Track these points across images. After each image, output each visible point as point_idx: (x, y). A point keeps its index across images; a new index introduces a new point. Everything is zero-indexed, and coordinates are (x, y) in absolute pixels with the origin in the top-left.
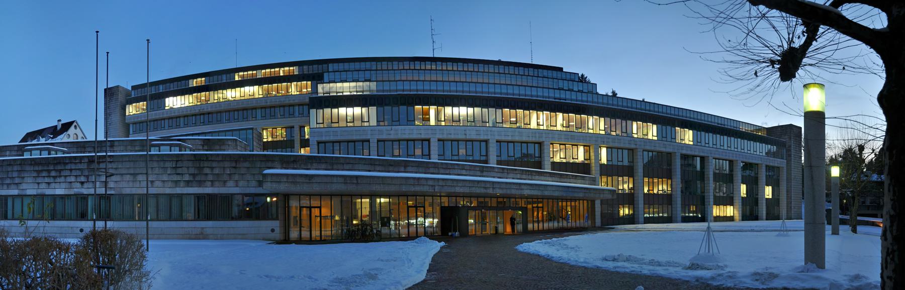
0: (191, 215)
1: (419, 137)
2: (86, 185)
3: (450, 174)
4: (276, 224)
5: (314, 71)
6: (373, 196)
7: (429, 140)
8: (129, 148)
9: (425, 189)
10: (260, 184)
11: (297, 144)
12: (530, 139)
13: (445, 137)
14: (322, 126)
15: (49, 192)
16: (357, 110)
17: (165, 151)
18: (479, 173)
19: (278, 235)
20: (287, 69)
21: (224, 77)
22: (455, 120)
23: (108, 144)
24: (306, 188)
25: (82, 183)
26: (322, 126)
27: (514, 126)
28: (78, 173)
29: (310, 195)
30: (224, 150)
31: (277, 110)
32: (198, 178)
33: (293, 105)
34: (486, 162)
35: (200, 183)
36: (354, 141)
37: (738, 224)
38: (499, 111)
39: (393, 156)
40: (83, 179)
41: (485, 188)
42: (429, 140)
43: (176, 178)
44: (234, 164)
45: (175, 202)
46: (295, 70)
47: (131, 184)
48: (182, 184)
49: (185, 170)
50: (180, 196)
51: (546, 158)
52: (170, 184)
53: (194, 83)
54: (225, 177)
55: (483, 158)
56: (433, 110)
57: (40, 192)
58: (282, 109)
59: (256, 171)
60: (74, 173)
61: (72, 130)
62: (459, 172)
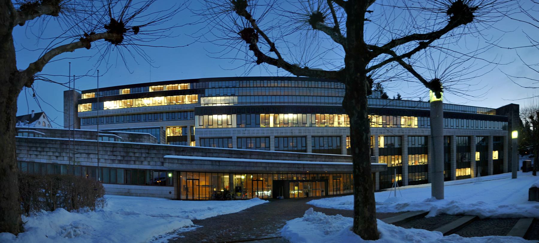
0: (123, 181)
2: (59, 158)
3: (278, 160)
4: (172, 189)
5: (199, 87)
6: (231, 174)
7: (269, 137)
8: (83, 136)
9: (261, 169)
10: (163, 163)
11: (189, 138)
13: (279, 135)
14: (202, 127)
15: (37, 160)
16: (224, 117)
17: (106, 140)
18: (297, 158)
19: (173, 195)
20: (183, 84)
21: (142, 88)
22: (285, 123)
23: (70, 132)
24: (189, 167)
25: (57, 157)
26: (202, 127)
27: (323, 126)
28: (54, 150)
30: (142, 142)
32: (126, 159)
33: (187, 112)
35: (128, 162)
36: (223, 138)
37: (473, 179)
38: (314, 116)
39: (247, 148)
40: (57, 154)
41: (298, 168)
42: (269, 137)
43: (113, 158)
44: (147, 151)
45: (112, 173)
46: (188, 86)
47: (86, 160)
48: (117, 162)
49: (118, 153)
50: (116, 169)
51: (344, 147)
52: (109, 161)
53: (123, 92)
54: (142, 159)
55: (304, 148)
56: (272, 116)
57: (32, 160)
58: (179, 114)
59: (160, 156)
61: (41, 119)
62: (284, 158)
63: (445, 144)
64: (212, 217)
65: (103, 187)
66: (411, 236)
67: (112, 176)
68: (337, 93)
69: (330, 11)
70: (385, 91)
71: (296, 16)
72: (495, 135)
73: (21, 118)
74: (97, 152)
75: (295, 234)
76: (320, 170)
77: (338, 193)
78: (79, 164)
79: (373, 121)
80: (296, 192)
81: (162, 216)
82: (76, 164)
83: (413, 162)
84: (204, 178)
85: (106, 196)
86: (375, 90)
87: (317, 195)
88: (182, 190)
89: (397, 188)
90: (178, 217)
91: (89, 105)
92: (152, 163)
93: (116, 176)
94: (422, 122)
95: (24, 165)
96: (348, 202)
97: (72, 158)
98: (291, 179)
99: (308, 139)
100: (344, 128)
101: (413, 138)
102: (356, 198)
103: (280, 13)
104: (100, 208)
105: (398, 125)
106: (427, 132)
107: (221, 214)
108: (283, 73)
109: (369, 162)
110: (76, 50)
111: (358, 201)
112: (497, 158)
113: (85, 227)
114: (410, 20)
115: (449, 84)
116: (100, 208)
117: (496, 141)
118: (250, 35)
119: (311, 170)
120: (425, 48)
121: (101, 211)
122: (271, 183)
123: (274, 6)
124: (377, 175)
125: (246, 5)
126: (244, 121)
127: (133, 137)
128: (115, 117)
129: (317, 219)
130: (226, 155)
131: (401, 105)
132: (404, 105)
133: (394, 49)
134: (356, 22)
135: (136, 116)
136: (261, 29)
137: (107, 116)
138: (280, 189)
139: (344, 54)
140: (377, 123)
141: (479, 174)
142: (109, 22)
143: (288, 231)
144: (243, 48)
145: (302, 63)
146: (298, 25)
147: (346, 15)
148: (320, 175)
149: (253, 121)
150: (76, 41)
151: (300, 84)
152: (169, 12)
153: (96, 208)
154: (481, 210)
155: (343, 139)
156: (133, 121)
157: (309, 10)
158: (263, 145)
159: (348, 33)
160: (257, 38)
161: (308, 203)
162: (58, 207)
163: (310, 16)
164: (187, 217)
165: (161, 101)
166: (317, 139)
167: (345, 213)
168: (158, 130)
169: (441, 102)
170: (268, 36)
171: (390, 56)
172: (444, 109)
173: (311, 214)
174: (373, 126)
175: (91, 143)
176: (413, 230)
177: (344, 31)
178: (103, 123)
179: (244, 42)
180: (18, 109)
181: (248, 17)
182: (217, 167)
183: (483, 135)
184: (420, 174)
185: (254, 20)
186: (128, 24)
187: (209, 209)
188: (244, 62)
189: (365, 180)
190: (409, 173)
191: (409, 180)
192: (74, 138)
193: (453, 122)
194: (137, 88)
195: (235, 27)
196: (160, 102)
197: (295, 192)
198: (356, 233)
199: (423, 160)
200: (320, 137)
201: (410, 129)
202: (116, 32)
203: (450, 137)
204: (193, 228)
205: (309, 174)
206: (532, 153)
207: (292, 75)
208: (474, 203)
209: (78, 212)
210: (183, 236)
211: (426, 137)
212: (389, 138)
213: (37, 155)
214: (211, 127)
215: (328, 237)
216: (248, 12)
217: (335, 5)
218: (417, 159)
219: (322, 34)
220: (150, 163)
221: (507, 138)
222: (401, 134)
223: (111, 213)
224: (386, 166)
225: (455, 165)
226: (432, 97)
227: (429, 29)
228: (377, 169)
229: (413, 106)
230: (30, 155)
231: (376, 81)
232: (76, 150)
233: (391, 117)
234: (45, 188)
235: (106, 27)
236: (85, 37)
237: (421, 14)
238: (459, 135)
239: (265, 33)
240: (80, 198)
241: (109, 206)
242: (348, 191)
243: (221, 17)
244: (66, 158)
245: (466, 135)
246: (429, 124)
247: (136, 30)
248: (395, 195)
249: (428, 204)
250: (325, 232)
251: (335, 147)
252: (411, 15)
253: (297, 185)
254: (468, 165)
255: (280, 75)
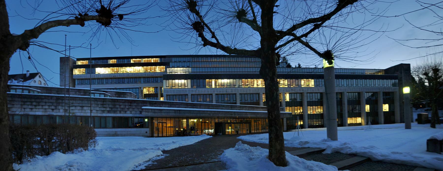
0: (111, 126)
1: (208, 93)
2: (55, 111)
4: (148, 130)
5: (166, 61)
6: (188, 118)
7: (212, 94)
8: (77, 93)
9: (207, 115)
10: (141, 113)
11: (159, 95)
12: (254, 92)
13: (218, 93)
14: (168, 88)
16: (183, 81)
17: (97, 96)
18: (230, 108)
20: (155, 59)
21: (126, 60)
22: (222, 85)
23: (66, 90)
24: (159, 115)
25: (53, 110)
27: (247, 87)
28: (50, 104)
29: (162, 118)
31: (150, 79)
32: (113, 109)
33: (157, 77)
34: (236, 103)
35: (115, 112)
36: (182, 95)
37: (364, 126)
38: (240, 80)
39: (198, 101)
40: (53, 107)
42: (212, 94)
43: (103, 109)
44: (130, 104)
45: (103, 121)
46: (158, 60)
47: (80, 111)
48: (106, 112)
49: (107, 106)
51: (261, 101)
52: (100, 112)
53: (111, 62)
54: (126, 110)
55: (235, 102)
56: (213, 81)
57: (25, 113)
59: (139, 107)
60: (48, 104)
61: (37, 78)
62: (222, 108)
63: (337, 98)
64: (175, 148)
65: (95, 131)
66: (311, 167)
67: (102, 123)
68: (256, 65)
69: (250, 8)
70: (289, 62)
71: (228, 13)
72: (385, 91)
73: (15, 77)
74: (89, 105)
75: (230, 159)
76: (245, 116)
77: (258, 131)
78: (73, 115)
79: (281, 83)
80: (230, 130)
81: (141, 150)
82: (71, 115)
83: (312, 111)
84: (169, 122)
85: (97, 138)
86: (282, 62)
87: (244, 132)
88: (155, 130)
89: (300, 130)
90: (152, 149)
91: (83, 70)
92: (133, 112)
93: (106, 123)
94: (318, 83)
95: (16, 118)
96: (265, 138)
97: (67, 110)
98: (227, 121)
99: (237, 96)
100: (261, 88)
101: (311, 94)
102: (270, 135)
103: (218, 11)
104: (93, 148)
105: (299, 85)
106: (322, 89)
107: (181, 146)
108: (221, 52)
109: (278, 111)
110: (71, 25)
111: (272, 137)
112: (387, 110)
113: (79, 164)
114: (307, 8)
115: (339, 53)
116: (93, 148)
117: (386, 95)
118: (199, 27)
119: (240, 116)
120: (318, 28)
121: (93, 150)
122: (213, 124)
123: (214, 6)
124: (285, 120)
125: (196, 5)
126: (195, 84)
127: (119, 94)
128: (105, 80)
129: (244, 149)
130: (184, 106)
131: (301, 71)
132: (303, 71)
133: (295, 32)
134: (268, 15)
135: (121, 79)
136: (206, 22)
137: (98, 79)
138: (220, 129)
139: (260, 38)
140: (284, 84)
141: (369, 123)
142: (100, 7)
143: (226, 157)
144: (194, 36)
145: (233, 46)
146: (229, 19)
147: (261, 10)
148: (245, 119)
149: (201, 84)
150: (72, 18)
151: (232, 59)
152: (145, 6)
153: (89, 148)
154: (373, 153)
155: (261, 95)
156: (119, 83)
157: (237, 8)
158: (208, 100)
159: (262, 23)
160: (203, 29)
161: (238, 138)
162: (53, 151)
163: (237, 13)
164: (159, 149)
165: (140, 69)
166: (243, 95)
167: (263, 146)
168: (137, 89)
169: (332, 67)
170: (210, 27)
171: (292, 37)
172: (335, 73)
173: (240, 145)
174: (281, 86)
175: (85, 99)
176: (312, 162)
177: (259, 22)
178: (95, 84)
179: (195, 32)
180: (11, 69)
181: (197, 13)
182: (178, 114)
183: (372, 91)
184: (317, 120)
185: (201, 16)
186: (114, 12)
187: (174, 142)
188: (195, 45)
189: (276, 123)
190: (308, 119)
191: (308, 124)
192: (69, 94)
193: (344, 82)
194: (121, 60)
195: (189, 20)
196: (138, 70)
197: (229, 130)
198: (270, 160)
199: (319, 110)
200: (245, 94)
201: (308, 88)
202: (105, 16)
203: (341, 93)
204: (163, 157)
205: (238, 118)
206: (429, 106)
207: (226, 54)
208: (366, 146)
209: (73, 153)
210: (156, 163)
211: (321, 94)
212: (293, 94)
213: (32, 109)
214: (174, 88)
215: (251, 162)
216: (197, 10)
217: (253, 3)
218: (314, 110)
219: (245, 25)
220: (129, 112)
221: (398, 93)
222: (302, 92)
223: (102, 150)
224: (291, 113)
225: (347, 115)
226: (326, 64)
227: (321, 13)
228: (285, 116)
229: (310, 71)
230: (24, 108)
231: (282, 56)
232: (71, 104)
233: (294, 80)
234: (40, 137)
235: (97, 11)
236: (79, 17)
237: (315, 3)
238: (349, 91)
239: (208, 25)
240: (75, 142)
241: (100, 145)
242: (265, 131)
243: (180, 13)
244: (61, 111)
245: (356, 91)
246: (323, 84)
247: (121, 17)
248: (298, 135)
249: (324, 143)
250: (249, 159)
251: (255, 101)
252: (307, 4)
253: (231, 126)
254: (359, 115)
255: (218, 54)
